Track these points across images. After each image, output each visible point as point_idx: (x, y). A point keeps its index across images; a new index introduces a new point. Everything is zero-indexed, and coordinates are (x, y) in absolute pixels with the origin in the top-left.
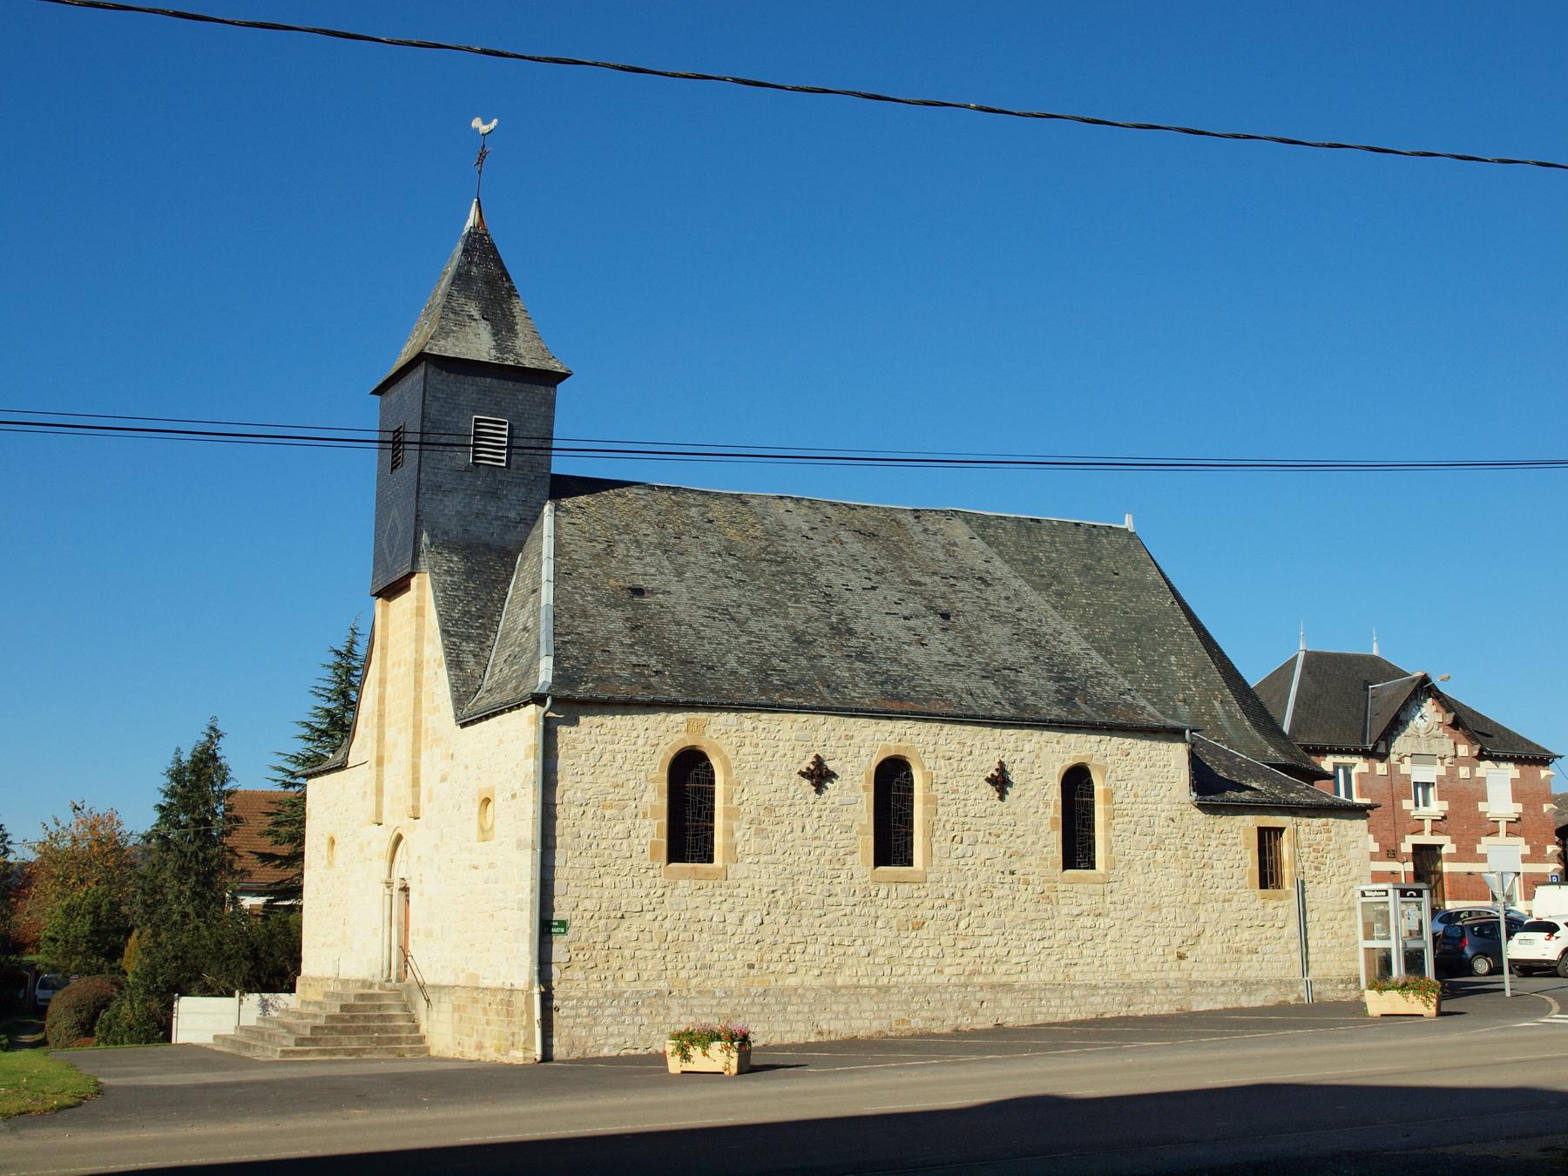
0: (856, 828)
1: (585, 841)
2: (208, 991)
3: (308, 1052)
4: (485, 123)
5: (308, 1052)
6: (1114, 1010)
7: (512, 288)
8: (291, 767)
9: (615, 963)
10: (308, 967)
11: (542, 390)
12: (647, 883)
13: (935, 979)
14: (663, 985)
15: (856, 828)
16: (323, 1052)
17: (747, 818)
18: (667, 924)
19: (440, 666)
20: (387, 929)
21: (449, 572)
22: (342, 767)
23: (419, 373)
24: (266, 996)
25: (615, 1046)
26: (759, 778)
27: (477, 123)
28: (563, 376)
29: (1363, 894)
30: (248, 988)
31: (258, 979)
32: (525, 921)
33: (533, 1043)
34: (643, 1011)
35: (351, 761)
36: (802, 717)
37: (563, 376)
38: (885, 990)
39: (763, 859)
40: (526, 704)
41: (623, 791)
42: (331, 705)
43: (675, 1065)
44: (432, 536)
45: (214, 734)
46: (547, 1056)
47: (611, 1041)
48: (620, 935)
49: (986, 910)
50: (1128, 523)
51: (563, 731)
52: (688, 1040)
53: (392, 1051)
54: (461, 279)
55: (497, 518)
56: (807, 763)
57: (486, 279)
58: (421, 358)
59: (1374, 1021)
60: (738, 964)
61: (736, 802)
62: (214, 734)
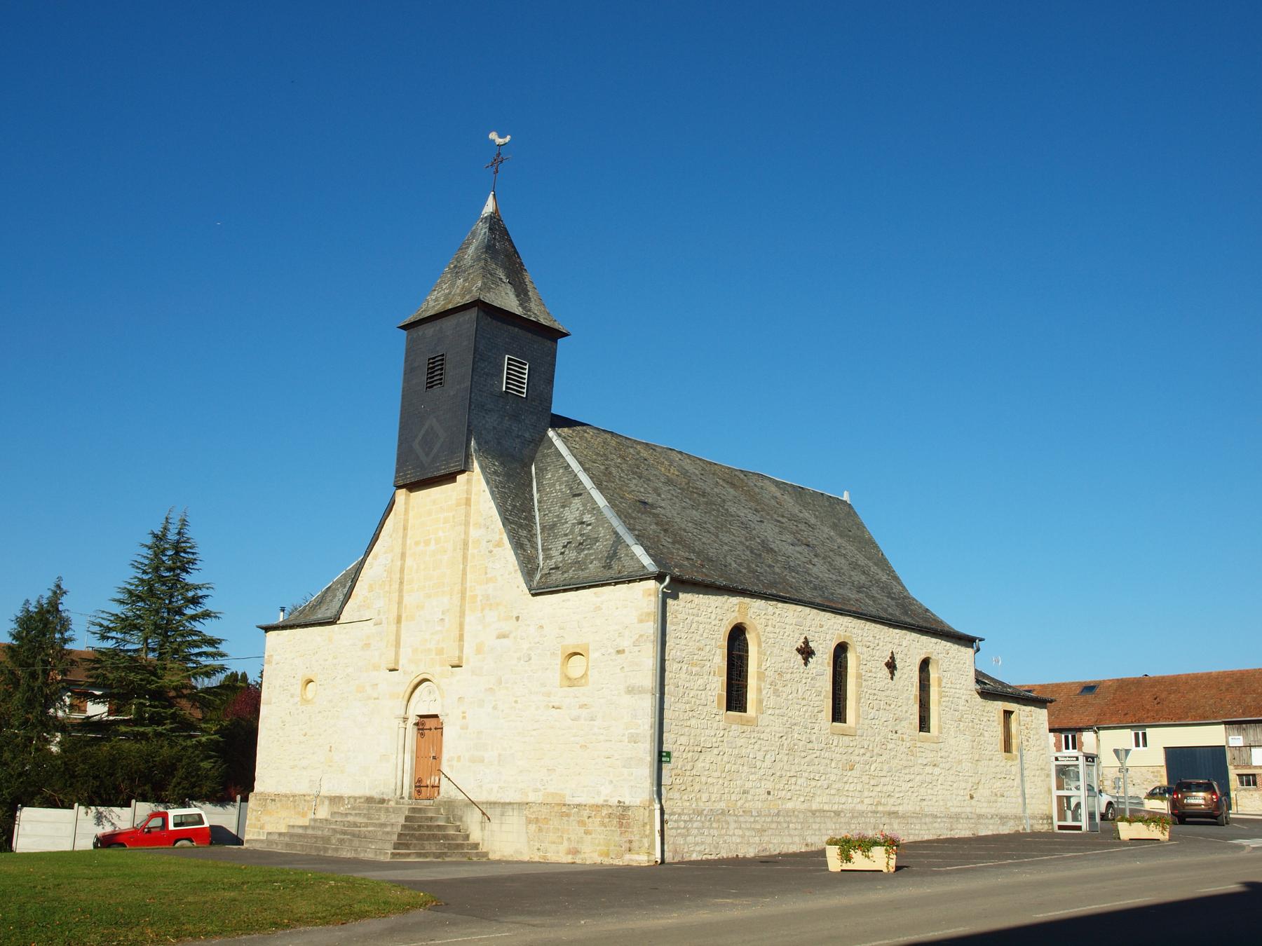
0: (824, 694)
1: (681, 690)
2: (51, 803)
3: (409, 855)
4: (500, 137)
5: (409, 855)
6: (962, 831)
7: (521, 264)
8: (106, 623)
9: (697, 788)
10: (258, 786)
11: (549, 343)
12: (715, 725)
13: (859, 807)
14: (723, 805)
15: (824, 694)
16: (419, 855)
17: (769, 680)
18: (725, 758)
19: (499, 544)
20: (400, 755)
21: (495, 473)
22: (333, 621)
23: (473, 313)
24: (101, 809)
25: (700, 852)
26: (776, 651)
27: (493, 136)
28: (565, 335)
29: (1057, 759)
30: (89, 803)
31: (100, 796)
32: (646, 751)
33: (654, 848)
34: (715, 825)
35: (343, 618)
36: (799, 608)
37: (565, 335)
38: (837, 813)
39: (777, 712)
40: (649, 579)
41: (703, 653)
42: (146, 577)
43: (834, 863)
44: (478, 443)
45: (59, 592)
46: (663, 861)
47: (698, 848)
48: (699, 765)
49: (884, 758)
50: (846, 497)
51: (670, 601)
52: (847, 846)
53: (464, 855)
54: (489, 248)
55: (518, 437)
56: (800, 643)
57: (502, 250)
58: (478, 303)
59: (1125, 843)
60: (762, 791)
61: (763, 667)
62: (59, 592)
